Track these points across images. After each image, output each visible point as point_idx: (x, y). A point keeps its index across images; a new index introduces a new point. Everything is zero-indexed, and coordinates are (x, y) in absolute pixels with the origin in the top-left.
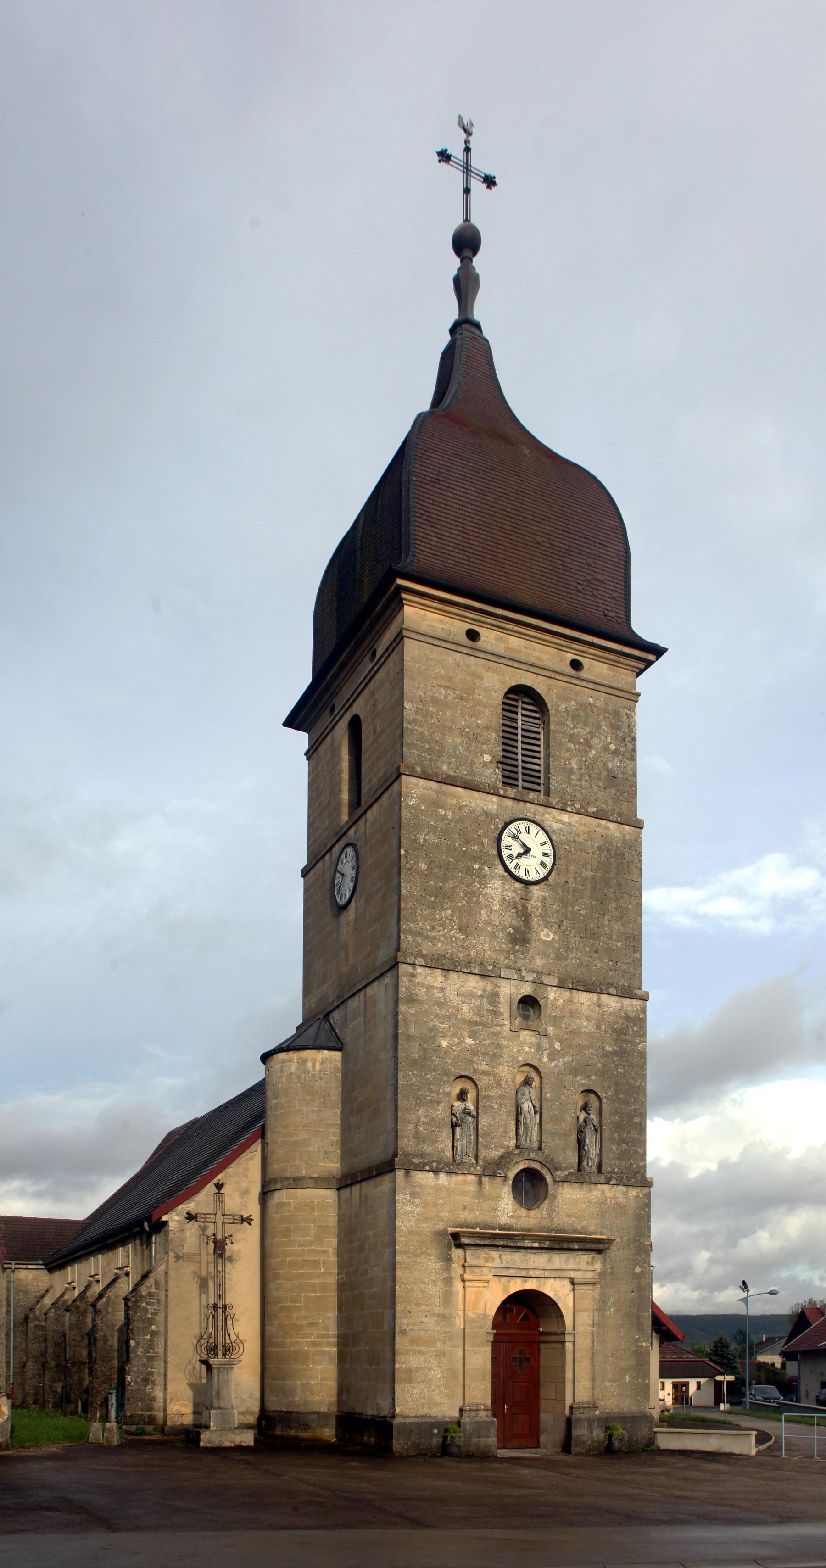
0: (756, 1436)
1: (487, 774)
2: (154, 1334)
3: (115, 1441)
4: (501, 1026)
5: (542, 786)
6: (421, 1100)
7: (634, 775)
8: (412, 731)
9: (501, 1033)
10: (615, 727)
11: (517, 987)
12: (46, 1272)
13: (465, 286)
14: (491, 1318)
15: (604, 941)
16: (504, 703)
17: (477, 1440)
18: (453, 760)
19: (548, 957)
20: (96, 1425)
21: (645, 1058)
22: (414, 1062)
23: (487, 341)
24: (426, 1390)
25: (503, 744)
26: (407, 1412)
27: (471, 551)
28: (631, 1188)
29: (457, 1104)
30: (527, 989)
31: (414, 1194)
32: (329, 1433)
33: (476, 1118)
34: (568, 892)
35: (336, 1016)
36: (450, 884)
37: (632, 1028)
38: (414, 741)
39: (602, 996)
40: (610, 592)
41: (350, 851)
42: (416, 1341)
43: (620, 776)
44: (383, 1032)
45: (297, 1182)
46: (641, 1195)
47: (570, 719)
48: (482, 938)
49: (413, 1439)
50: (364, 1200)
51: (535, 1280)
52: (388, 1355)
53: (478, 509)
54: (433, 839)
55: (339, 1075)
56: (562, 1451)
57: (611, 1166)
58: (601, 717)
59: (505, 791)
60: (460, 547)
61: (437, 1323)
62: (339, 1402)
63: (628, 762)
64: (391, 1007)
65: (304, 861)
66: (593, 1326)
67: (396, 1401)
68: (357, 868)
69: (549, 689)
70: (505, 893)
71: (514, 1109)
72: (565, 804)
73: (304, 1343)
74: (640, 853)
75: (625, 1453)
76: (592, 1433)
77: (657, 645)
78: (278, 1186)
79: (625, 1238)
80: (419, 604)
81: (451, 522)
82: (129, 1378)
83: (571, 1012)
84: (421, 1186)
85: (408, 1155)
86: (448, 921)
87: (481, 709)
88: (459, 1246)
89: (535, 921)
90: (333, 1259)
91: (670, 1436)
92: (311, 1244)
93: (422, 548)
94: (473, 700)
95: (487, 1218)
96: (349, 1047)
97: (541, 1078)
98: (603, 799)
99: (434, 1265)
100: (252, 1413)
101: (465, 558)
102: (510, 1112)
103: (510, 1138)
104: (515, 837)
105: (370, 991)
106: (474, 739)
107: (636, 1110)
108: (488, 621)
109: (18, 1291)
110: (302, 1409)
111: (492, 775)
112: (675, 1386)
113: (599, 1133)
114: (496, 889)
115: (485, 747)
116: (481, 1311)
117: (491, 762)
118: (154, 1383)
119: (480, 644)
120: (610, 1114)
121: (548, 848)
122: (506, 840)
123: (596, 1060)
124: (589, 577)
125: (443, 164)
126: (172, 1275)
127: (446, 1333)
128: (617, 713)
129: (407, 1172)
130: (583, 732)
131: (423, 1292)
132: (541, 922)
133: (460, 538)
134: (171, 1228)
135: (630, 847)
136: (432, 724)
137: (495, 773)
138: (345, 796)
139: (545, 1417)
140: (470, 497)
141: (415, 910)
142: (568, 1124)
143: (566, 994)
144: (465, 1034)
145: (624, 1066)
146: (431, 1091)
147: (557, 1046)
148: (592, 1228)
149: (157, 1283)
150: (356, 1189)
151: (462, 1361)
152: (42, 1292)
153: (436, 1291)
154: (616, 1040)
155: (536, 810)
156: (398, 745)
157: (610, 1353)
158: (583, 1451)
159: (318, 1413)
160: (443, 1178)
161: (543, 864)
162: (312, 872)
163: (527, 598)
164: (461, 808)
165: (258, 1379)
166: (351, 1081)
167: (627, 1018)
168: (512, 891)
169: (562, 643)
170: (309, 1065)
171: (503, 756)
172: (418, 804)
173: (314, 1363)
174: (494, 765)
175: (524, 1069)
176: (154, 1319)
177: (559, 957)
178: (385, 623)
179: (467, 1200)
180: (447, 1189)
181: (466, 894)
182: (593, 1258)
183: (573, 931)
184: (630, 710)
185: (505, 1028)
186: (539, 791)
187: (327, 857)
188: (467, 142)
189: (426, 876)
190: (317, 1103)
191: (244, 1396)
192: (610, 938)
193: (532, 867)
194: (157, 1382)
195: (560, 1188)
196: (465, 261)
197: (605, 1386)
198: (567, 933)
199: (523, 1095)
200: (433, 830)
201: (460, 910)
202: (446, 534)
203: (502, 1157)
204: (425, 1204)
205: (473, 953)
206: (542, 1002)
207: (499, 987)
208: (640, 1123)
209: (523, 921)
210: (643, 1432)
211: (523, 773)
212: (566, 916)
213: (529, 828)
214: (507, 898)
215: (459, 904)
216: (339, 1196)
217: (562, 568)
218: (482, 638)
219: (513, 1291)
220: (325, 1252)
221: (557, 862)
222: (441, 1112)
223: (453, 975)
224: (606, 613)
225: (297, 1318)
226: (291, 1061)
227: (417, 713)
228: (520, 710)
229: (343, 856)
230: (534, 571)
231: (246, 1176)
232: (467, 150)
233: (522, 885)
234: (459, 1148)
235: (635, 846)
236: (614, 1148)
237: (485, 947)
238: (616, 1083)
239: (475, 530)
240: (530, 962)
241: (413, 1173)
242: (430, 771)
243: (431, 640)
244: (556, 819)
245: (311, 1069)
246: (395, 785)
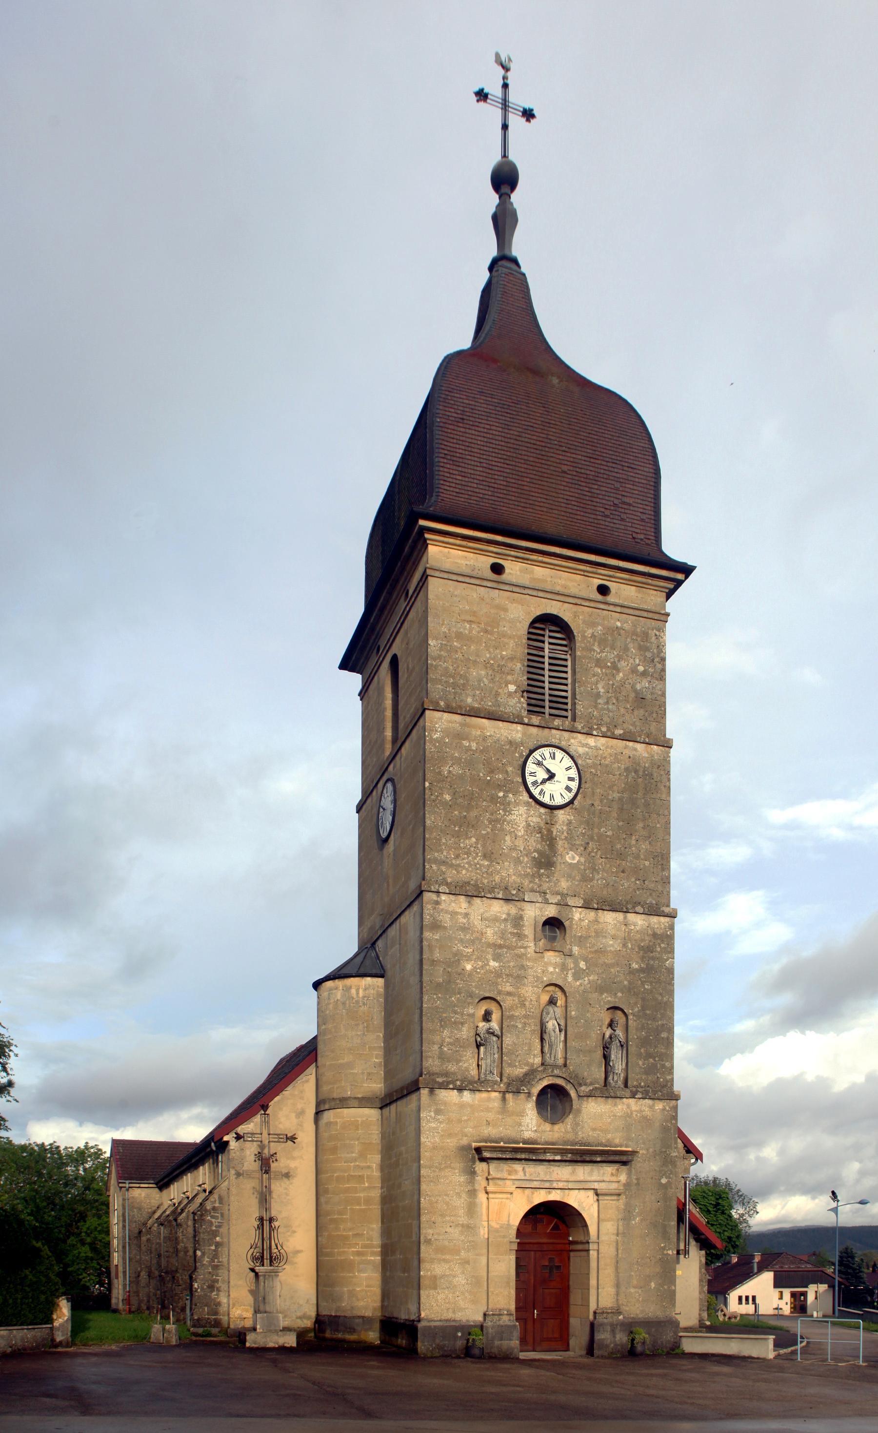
0: (774, 1340)
1: (512, 704)
2: (218, 1245)
3: (174, 1342)
4: (525, 948)
5: (570, 712)
6: (445, 1022)
7: (664, 695)
8: (436, 667)
9: (525, 955)
10: (643, 649)
11: (541, 909)
12: (157, 1190)
13: (504, 222)
14: (515, 1228)
15: (631, 861)
16: (529, 633)
17: (499, 1342)
18: (478, 692)
19: (574, 879)
20: (157, 1327)
21: (673, 974)
22: (439, 985)
23: (524, 275)
24: (450, 1296)
25: (529, 672)
26: (432, 1316)
27: (496, 486)
28: (657, 1101)
29: (482, 1024)
30: (551, 911)
31: (438, 1112)
32: (373, 1336)
33: (500, 1037)
34: (594, 814)
35: (380, 944)
36: (474, 813)
37: (659, 945)
38: (439, 677)
39: (629, 915)
40: (639, 514)
41: (389, 786)
42: (441, 1250)
43: (649, 697)
44: (412, 958)
45: (343, 1102)
46: (667, 1108)
47: (596, 644)
49: (437, 1341)
50: (399, 1117)
51: (558, 1191)
52: (416, 1263)
53: (503, 444)
54: (457, 770)
55: (382, 1000)
56: (587, 1354)
57: (637, 1080)
58: (629, 640)
59: (530, 719)
60: (484, 483)
61: (462, 1233)
62: (383, 1307)
64: (418, 934)
65: (358, 797)
66: (617, 1235)
67: (422, 1305)
68: (395, 801)
69: (576, 615)
70: (530, 819)
71: (539, 1028)
72: (591, 728)
73: (349, 1253)
74: (669, 772)
75: (648, 1355)
76: (614, 1337)
77: (686, 564)
78: (327, 1107)
79: (651, 1150)
80: (443, 542)
81: (476, 459)
82: (196, 1285)
83: (596, 932)
84: (445, 1104)
85: (433, 1074)
86: (472, 849)
87: (506, 640)
88: (483, 1160)
89: (560, 844)
90: (377, 1174)
91: (694, 1339)
92: (355, 1160)
93: (446, 488)
94: (498, 632)
95: (510, 1133)
96: (389, 973)
97: (566, 996)
98: (631, 721)
99: (458, 1178)
100: (309, 1318)
101: (490, 493)
102: (534, 1031)
103: (534, 1055)
104: (539, 764)
105: (403, 919)
106: (499, 670)
107: (663, 1025)
108: (512, 553)
109: (132, 1208)
110: (348, 1314)
111: (517, 704)
112: (793, 1295)
113: (625, 1049)
114: (522, 816)
115: (509, 678)
116: (504, 1220)
117: (515, 692)
118: (218, 1290)
119: (504, 577)
120: (637, 1029)
121: (573, 773)
122: (530, 767)
123: (622, 977)
124: (616, 501)
125: (482, 104)
126: (234, 1190)
128: (646, 635)
129: (432, 1090)
130: (610, 655)
131: (447, 1204)
132: (566, 845)
133: (485, 474)
134: (232, 1148)
135: (659, 767)
136: (456, 659)
137: (520, 702)
138: (389, 733)
139: (574, 1322)
140: (494, 432)
141: (440, 840)
142: (593, 1041)
143: (592, 914)
144: (489, 957)
145: (651, 983)
146: (456, 1013)
147: (582, 965)
148: (617, 1141)
149: (221, 1199)
150: (393, 1107)
151: (486, 1268)
152: (154, 1209)
153: (460, 1202)
154: (643, 958)
155: (561, 736)
156: (424, 682)
157: (635, 1260)
158: (606, 1354)
159: (363, 1317)
160: (467, 1095)
161: (568, 789)
162: (364, 807)
163: (551, 528)
164: (485, 739)
165: (315, 1286)
166: (392, 1003)
167: (655, 935)
168: (537, 816)
170: (353, 991)
171: (529, 685)
172: (443, 738)
173: (359, 1271)
174: (519, 694)
175: (548, 988)
176: (218, 1231)
177: (585, 879)
178: (414, 563)
179: (491, 1116)
180: (471, 1106)
181: (490, 823)
182: (618, 1170)
183: (599, 853)
184: (659, 631)
185: (529, 950)
186: (567, 717)
187: (374, 793)
188: (505, 78)
189: (450, 806)
190: (361, 1027)
191: (301, 1302)
192: (637, 857)
193: (557, 792)
194: (222, 1289)
195: (585, 1103)
196: (503, 197)
198: (593, 854)
199: (548, 1013)
200: (457, 761)
201: (485, 838)
202: (470, 471)
203: (526, 1074)
204: (450, 1121)
205: (497, 878)
206: (566, 924)
207: (523, 910)
208: (668, 1038)
209: (548, 845)
210: (668, 1337)
211: (547, 700)
212: (592, 839)
213: (554, 754)
215: (483, 832)
216: (382, 1115)
217: (589, 494)
218: (507, 571)
219: (537, 1201)
220: (369, 1167)
221: (582, 786)
222: (466, 1033)
223: (477, 901)
224: (635, 535)
225: (344, 1230)
226: (336, 988)
227: (441, 650)
228: (547, 639)
229: (385, 791)
230: (559, 500)
231: (302, 1098)
232: (505, 86)
233: (547, 810)
234: (484, 1067)
235: (663, 766)
236: (641, 1063)
237: (509, 872)
238: (643, 999)
239: (499, 464)
240: (555, 884)
241: (437, 1091)
242: (454, 705)
243: (455, 577)
244: (580, 743)
245: (355, 996)
246: (421, 720)
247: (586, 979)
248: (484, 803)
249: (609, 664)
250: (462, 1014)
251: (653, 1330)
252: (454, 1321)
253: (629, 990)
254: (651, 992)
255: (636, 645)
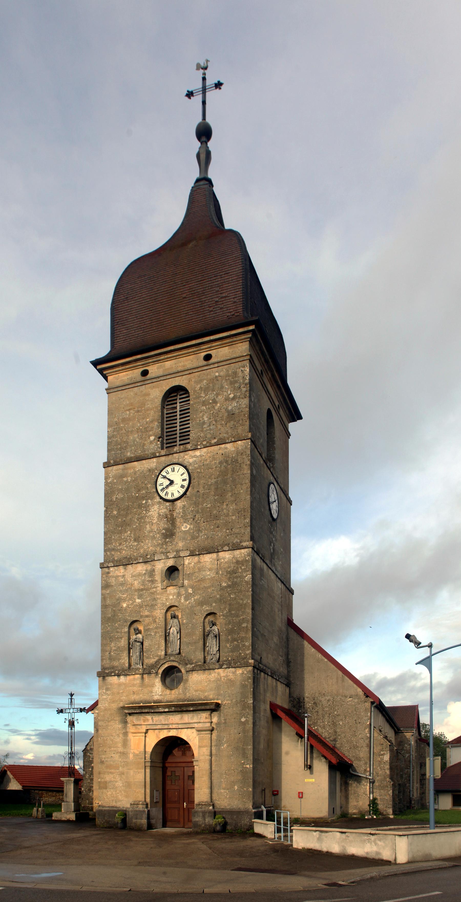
1: (152, 447)
4: (156, 588)
13: (204, 158)
15: (223, 519)
18: (133, 448)
24: (114, 793)
26: (105, 804)
28: (238, 669)
30: (170, 563)
36: (130, 517)
37: (241, 567)
38: (113, 447)
42: (109, 767)
46: (245, 672)
47: (203, 392)
48: (147, 541)
49: (106, 818)
51: (175, 730)
54: (120, 496)
57: (226, 657)
58: (223, 381)
63: (242, 400)
71: (164, 633)
76: (205, 820)
79: (234, 700)
80: (114, 372)
84: (111, 684)
86: (128, 538)
99: (118, 725)
102: (161, 635)
104: (165, 477)
108: (150, 361)
113: (218, 638)
114: (156, 510)
115: (151, 433)
117: (154, 440)
121: (186, 476)
127: (124, 762)
131: (112, 740)
132: (182, 521)
135: (242, 453)
141: (111, 537)
143: (196, 558)
144: (136, 597)
145: (235, 593)
146: (118, 632)
147: (190, 591)
148: (211, 697)
153: (119, 739)
155: (179, 456)
157: (224, 771)
161: (182, 486)
164: (135, 473)
167: (238, 562)
169: (195, 349)
172: (113, 480)
177: (193, 538)
179: (135, 689)
180: (124, 684)
181: (138, 520)
183: (203, 519)
185: (158, 588)
193: (176, 491)
197: (221, 793)
198: (198, 521)
201: (135, 530)
204: (113, 694)
205: (142, 551)
206: (180, 568)
209: (171, 524)
212: (198, 512)
214: (161, 514)
219: (162, 737)
221: (192, 482)
223: (130, 567)
227: (114, 431)
233: (170, 503)
236: (228, 645)
237: (148, 546)
238: (230, 605)
247: (193, 599)
248: (135, 510)
249: (211, 401)
250: (121, 632)
251: (235, 817)
252: (116, 807)
253: (220, 600)
254: (235, 598)
255: (229, 382)
